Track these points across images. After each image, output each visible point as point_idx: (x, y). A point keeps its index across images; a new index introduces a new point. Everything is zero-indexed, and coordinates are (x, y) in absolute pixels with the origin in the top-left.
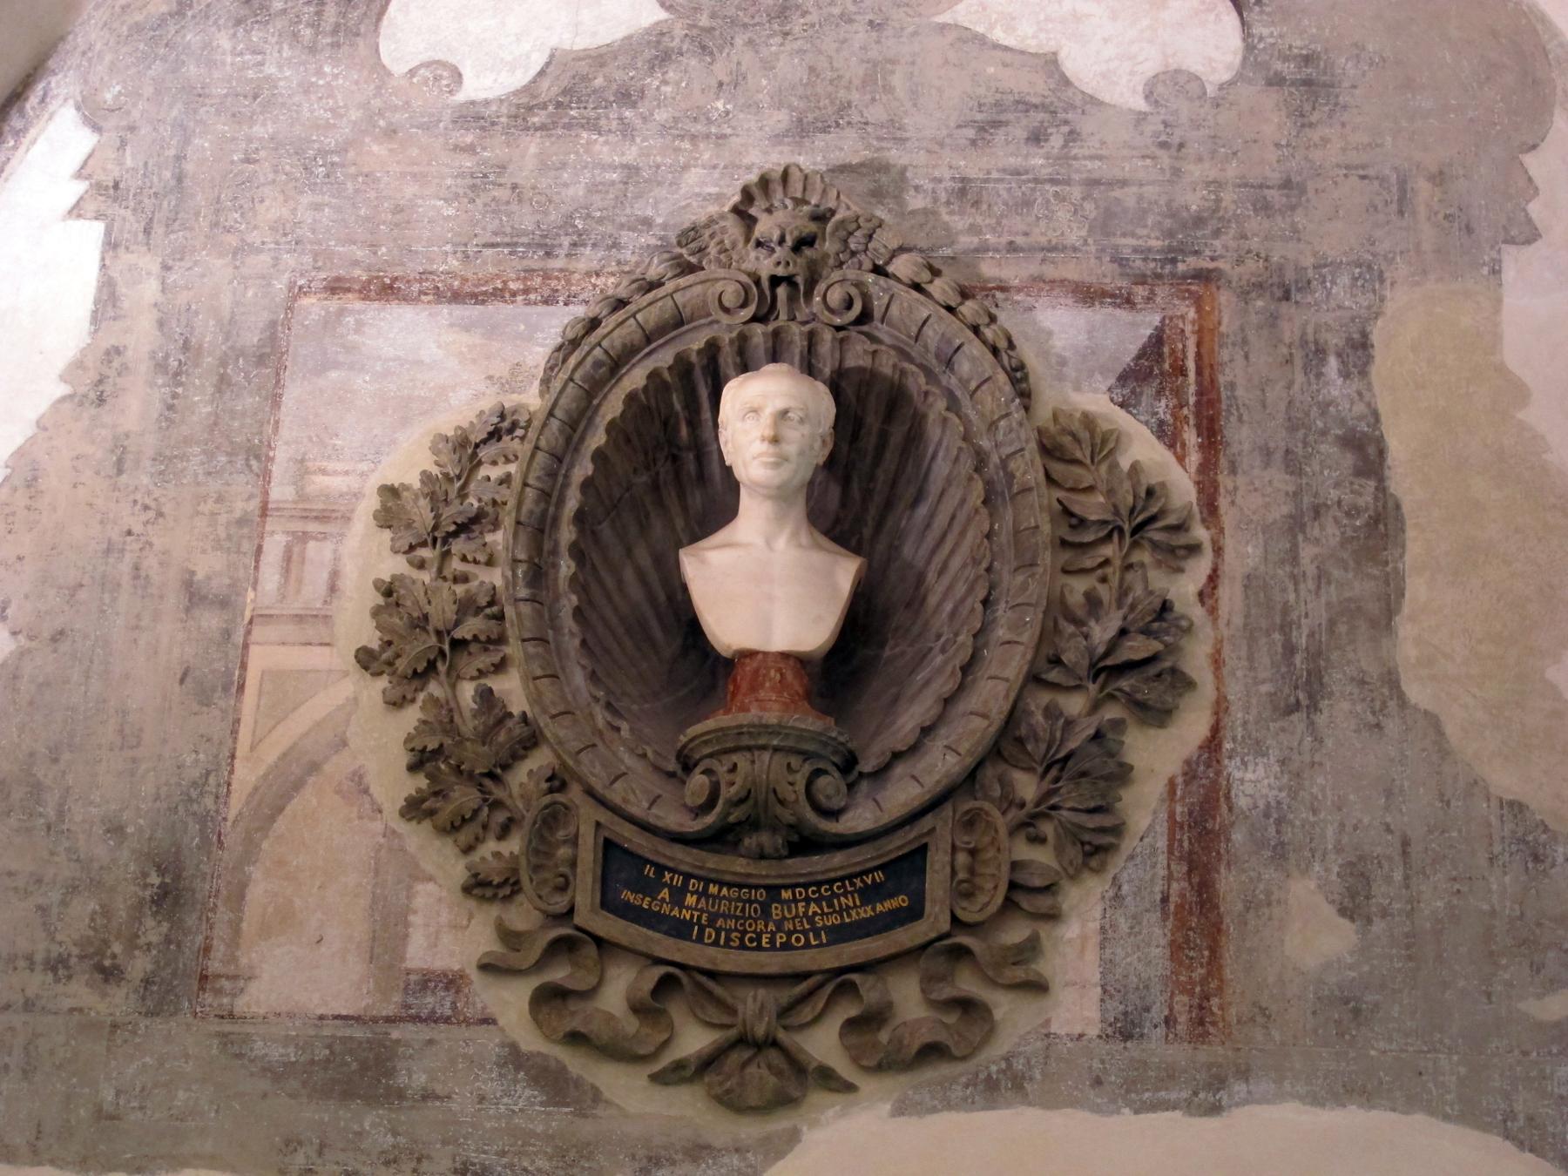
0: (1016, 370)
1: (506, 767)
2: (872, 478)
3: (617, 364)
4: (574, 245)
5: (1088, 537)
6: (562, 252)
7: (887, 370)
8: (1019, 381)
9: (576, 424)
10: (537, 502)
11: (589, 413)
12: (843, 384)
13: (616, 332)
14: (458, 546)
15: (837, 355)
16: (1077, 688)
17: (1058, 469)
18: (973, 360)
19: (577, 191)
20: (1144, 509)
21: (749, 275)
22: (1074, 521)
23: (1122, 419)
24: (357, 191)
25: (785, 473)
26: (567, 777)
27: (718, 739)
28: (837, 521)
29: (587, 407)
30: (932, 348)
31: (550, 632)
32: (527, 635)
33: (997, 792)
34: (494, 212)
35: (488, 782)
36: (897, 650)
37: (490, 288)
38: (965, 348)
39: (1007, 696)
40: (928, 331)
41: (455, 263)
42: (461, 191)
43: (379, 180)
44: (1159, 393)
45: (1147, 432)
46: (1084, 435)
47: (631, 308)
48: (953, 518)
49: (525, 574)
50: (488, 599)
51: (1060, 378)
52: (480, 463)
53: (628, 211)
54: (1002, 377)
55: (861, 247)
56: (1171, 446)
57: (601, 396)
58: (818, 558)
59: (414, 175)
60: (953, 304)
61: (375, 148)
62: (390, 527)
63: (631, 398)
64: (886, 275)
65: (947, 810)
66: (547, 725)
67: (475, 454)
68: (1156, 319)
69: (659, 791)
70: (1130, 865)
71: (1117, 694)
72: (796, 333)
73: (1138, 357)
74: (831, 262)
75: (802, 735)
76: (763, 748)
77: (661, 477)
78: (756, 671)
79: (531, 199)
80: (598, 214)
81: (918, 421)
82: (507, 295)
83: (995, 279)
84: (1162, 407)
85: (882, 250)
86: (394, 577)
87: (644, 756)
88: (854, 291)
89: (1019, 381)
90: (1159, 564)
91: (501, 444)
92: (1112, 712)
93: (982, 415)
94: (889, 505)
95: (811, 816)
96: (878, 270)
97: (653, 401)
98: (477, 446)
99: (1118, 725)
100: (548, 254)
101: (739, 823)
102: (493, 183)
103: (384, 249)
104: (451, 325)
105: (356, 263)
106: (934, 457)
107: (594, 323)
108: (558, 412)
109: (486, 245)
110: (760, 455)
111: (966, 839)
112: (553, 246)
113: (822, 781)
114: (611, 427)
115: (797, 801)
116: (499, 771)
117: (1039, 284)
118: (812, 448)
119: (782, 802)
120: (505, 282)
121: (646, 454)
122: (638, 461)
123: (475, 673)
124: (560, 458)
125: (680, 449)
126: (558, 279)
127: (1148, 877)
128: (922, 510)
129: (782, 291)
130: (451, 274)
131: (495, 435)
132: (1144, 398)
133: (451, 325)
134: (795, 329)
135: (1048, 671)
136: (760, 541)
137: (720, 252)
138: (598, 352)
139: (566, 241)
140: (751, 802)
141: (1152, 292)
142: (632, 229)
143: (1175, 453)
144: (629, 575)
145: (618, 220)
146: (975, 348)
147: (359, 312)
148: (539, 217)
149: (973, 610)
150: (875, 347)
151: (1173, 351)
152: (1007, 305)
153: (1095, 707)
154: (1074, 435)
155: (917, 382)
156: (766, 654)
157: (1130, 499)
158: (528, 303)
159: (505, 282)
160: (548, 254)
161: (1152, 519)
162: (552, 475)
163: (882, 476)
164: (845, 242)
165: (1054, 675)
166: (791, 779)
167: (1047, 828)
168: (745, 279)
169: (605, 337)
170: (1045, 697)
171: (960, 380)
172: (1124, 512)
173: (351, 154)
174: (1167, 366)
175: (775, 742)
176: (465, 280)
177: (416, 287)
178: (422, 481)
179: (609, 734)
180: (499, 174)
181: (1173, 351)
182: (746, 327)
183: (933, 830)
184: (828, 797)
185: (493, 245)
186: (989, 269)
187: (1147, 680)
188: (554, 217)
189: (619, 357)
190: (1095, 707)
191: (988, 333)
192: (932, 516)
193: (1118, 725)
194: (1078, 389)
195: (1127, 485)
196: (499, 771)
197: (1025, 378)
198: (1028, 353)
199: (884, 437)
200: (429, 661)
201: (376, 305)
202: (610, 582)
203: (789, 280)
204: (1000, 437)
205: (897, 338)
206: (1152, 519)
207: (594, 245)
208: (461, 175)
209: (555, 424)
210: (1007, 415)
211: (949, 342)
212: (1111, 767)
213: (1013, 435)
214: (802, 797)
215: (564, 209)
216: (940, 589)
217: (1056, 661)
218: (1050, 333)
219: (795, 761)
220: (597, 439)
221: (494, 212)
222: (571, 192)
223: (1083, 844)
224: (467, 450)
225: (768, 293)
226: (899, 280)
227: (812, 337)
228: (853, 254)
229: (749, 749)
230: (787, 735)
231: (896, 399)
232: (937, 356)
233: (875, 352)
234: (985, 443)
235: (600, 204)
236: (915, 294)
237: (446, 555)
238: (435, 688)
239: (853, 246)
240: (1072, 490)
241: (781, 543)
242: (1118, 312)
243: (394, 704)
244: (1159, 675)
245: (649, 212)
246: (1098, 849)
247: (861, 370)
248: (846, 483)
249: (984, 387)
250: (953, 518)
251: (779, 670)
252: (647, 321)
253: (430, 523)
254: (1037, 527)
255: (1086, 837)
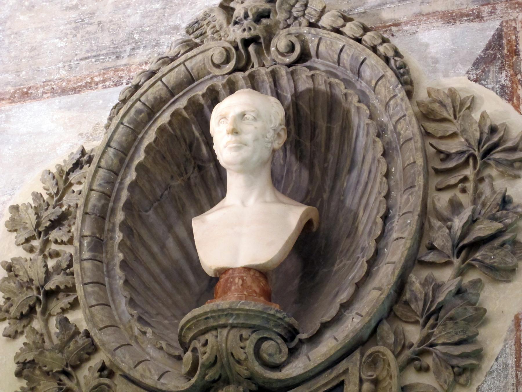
0: (399, 68)
1: (76, 367)
2: (325, 160)
3: (152, 111)
4: (133, 49)
5: (451, 164)
6: (126, 55)
7: (323, 87)
8: (403, 75)
9: (125, 152)
10: (99, 199)
11: (136, 144)
12: (301, 103)
13: (151, 93)
14: (54, 235)
15: (292, 84)
16: (448, 263)
17: (432, 127)
18: (373, 67)
19: (136, 19)
20: (488, 140)
21: (231, 43)
22: (442, 156)
23: (477, 89)
24: (10, 43)
25: (245, 153)
26: (114, 369)
27: (195, 324)
28: (308, 192)
29: (135, 140)
30: (348, 67)
31: (106, 279)
32: (87, 280)
33: (391, 339)
34: (87, 39)
35: (63, 377)
36: (341, 265)
37: (83, 83)
38: (367, 61)
39: (393, 273)
40: (344, 55)
41: (64, 72)
42: (69, 32)
43: (23, 34)
44: (501, 69)
45: (493, 94)
46: (448, 101)
47: (158, 75)
48: (370, 172)
49: (89, 244)
50: (67, 263)
51: (435, 71)
52: (71, 185)
53: (165, 24)
54: (390, 73)
55: (300, 14)
56: (510, 100)
57: (143, 131)
58: (277, 208)
59: (42, 28)
60: (357, 35)
61: (22, 18)
62: (16, 230)
63: (162, 130)
64: (318, 27)
65: (357, 355)
66: (95, 334)
67: (67, 179)
68: (497, 24)
69: (168, 369)
70: (489, 378)
71: (473, 262)
72: (263, 73)
73: (487, 49)
74: (281, 26)
75: (248, 314)
76: (224, 326)
77: (192, 181)
78: (227, 280)
79: (109, 29)
80: (148, 29)
81: (347, 113)
82: (93, 85)
83: (391, 20)
84: (503, 78)
85: (314, 13)
86: (13, 259)
87: (161, 348)
88: (294, 39)
89: (403, 75)
90: (503, 174)
91: (83, 171)
92: (473, 276)
93: (381, 101)
94: (336, 176)
95: (258, 368)
96: (311, 25)
97: (178, 132)
98: (68, 174)
99: (477, 284)
100: (117, 57)
101: (214, 381)
102: (87, 24)
103: (24, 73)
104: (60, 108)
105: (8, 84)
106: (357, 137)
107: (137, 87)
108: (113, 144)
109: (82, 59)
110: (228, 143)
111: (370, 373)
112: (121, 52)
113: (265, 345)
114: (149, 150)
115: (246, 359)
116: (70, 369)
117: (420, 17)
118: (264, 136)
119: (239, 362)
120: (92, 78)
121: (179, 167)
122: (165, 164)
123: (60, 311)
124: (115, 173)
125: (203, 161)
126: (123, 70)
127: (502, 385)
128: (355, 174)
129: (251, 48)
130: (61, 79)
131: (78, 165)
132: (491, 75)
133: (60, 108)
134: (263, 71)
135: (427, 254)
136: (238, 203)
137: (213, 33)
138: (138, 105)
139: (128, 48)
140: (218, 364)
141: (494, 8)
142: (168, 33)
143: (513, 104)
144: (171, 243)
145: (159, 30)
146: (373, 59)
147: (8, 111)
148: (113, 37)
149: (375, 223)
150: (312, 72)
151: (509, 41)
152: (400, 34)
153: (461, 273)
154: (441, 103)
155: (340, 89)
156: (234, 269)
157: (478, 135)
158: (105, 87)
159: (92, 78)
160: (117, 57)
161: (496, 146)
162: (111, 183)
163: (331, 157)
164: (290, 12)
165: (430, 257)
166: (242, 344)
167: (429, 361)
168: (227, 45)
169: (142, 95)
170: (425, 273)
171: (367, 83)
172: (474, 144)
173: (8, 24)
174: (505, 51)
175: (230, 321)
176: (69, 81)
177: (41, 91)
178: (34, 200)
179: (141, 337)
180: (91, 18)
181: (509, 41)
182: (232, 76)
183: (346, 371)
184: (270, 355)
185: (86, 58)
186: (387, 15)
187: (492, 249)
188: (122, 35)
189: (153, 106)
190: (461, 273)
191: (381, 49)
192: (359, 175)
193: (477, 284)
194: (446, 76)
195: (476, 126)
196: (70, 369)
197: (408, 72)
198: (414, 62)
199: (329, 131)
200: (30, 306)
201: (18, 104)
202: (155, 249)
203: (254, 40)
204: (391, 112)
205: (327, 65)
206: (496, 146)
207: (145, 47)
208: (69, 23)
209: (111, 151)
210: (394, 96)
211: (357, 59)
212: (470, 312)
213: (398, 108)
214: (252, 357)
215: (128, 30)
216: (364, 220)
217: (432, 248)
218: (427, 45)
219: (245, 333)
220: (141, 157)
221: (87, 39)
222: (132, 19)
223: (453, 367)
224: (63, 180)
225: (242, 51)
226: (324, 28)
227: (274, 74)
228: (296, 18)
229: (215, 328)
230: (238, 316)
231: (332, 105)
232: (352, 71)
233: (313, 76)
234: (385, 119)
235: (149, 23)
236: (334, 34)
237: (47, 242)
238: (37, 324)
239: (295, 14)
240: (442, 138)
241: (251, 201)
242: (472, 24)
243: (9, 336)
244: (503, 245)
245: (178, 22)
246: (464, 370)
247: (309, 90)
248: (311, 168)
249: (380, 83)
250: (370, 172)
251: (242, 278)
252: (169, 82)
253: (34, 222)
254: (414, 162)
255: (455, 362)
